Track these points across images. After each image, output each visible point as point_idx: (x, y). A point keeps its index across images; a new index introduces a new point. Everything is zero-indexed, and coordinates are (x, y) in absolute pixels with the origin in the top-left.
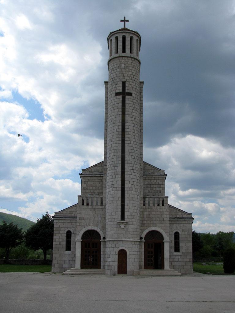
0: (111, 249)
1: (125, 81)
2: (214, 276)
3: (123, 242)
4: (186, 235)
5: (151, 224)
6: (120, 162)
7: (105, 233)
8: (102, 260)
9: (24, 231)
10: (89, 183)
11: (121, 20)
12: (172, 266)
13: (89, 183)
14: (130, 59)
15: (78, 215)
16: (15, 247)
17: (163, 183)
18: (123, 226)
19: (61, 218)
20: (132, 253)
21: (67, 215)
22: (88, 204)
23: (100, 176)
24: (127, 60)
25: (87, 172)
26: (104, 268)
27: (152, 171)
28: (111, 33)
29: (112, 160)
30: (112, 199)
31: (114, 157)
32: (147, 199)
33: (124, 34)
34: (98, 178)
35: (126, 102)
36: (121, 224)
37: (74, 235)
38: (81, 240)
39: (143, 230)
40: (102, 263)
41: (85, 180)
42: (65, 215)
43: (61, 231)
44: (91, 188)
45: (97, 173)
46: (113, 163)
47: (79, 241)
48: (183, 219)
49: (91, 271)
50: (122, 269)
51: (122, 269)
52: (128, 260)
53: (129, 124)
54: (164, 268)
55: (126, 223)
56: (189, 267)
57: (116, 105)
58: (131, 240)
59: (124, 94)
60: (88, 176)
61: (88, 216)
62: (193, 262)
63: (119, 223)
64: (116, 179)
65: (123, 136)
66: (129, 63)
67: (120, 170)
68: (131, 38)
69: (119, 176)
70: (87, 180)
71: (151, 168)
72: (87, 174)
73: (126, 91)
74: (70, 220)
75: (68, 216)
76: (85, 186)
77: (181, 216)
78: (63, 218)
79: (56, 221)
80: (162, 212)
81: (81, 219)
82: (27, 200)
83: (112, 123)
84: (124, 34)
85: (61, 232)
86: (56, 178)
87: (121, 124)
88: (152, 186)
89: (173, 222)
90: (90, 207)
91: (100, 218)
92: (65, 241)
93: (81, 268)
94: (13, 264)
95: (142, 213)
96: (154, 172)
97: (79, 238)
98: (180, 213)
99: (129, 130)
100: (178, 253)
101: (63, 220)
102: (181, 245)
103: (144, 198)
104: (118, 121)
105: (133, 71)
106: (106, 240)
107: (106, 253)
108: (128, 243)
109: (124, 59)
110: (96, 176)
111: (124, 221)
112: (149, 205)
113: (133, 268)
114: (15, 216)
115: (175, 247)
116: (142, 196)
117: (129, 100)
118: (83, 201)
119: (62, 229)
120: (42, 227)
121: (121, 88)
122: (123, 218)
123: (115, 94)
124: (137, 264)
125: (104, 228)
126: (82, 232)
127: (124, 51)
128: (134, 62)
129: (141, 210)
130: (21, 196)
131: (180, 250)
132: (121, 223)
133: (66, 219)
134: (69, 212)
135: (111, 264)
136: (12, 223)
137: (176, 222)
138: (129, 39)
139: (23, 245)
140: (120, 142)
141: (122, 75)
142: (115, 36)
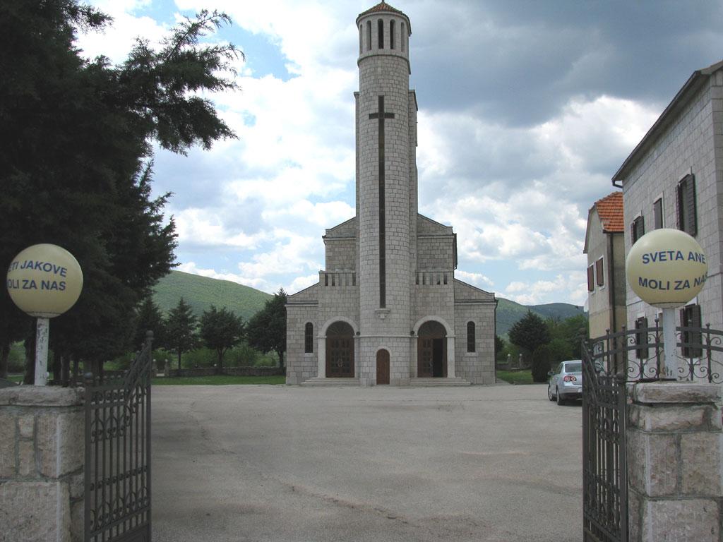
0: (366, 349)
7: (359, 325)
8: (356, 364)
9: (245, 322)
12: (457, 372)
14: (391, 58)
15: (320, 301)
16: (231, 348)
18: (382, 316)
20: (397, 354)
21: (305, 300)
22: (333, 284)
24: (386, 61)
26: (359, 377)
27: (433, 229)
28: (360, 15)
30: (367, 277)
32: (421, 275)
33: (381, 17)
35: (386, 129)
37: (316, 329)
39: (416, 321)
40: (356, 370)
42: (307, 298)
44: (340, 258)
50: (383, 377)
51: (383, 377)
52: (391, 365)
53: (390, 163)
54: (446, 376)
56: (490, 373)
57: (370, 133)
59: (381, 116)
61: (334, 301)
66: (388, 65)
67: (378, 234)
68: (392, 23)
69: (377, 242)
71: (430, 225)
72: (333, 236)
73: (385, 111)
76: (331, 254)
77: (478, 298)
79: (291, 309)
81: (324, 306)
82: (253, 248)
83: (365, 161)
84: (381, 17)
85: (298, 325)
86: (314, 199)
87: (377, 164)
88: (433, 252)
89: (465, 307)
90: (338, 288)
94: (230, 375)
95: (413, 296)
96: (435, 231)
98: (476, 294)
99: (391, 172)
100: (473, 354)
102: (477, 341)
103: (417, 273)
104: (373, 159)
105: (395, 78)
106: (361, 336)
108: (391, 340)
109: (381, 60)
111: (384, 309)
113: (398, 376)
114: (231, 283)
115: (468, 344)
116: (413, 270)
117: (390, 125)
118: (327, 277)
119: (299, 320)
120: (275, 314)
121: (377, 106)
122: (383, 303)
123: (368, 116)
124: (406, 370)
125: (357, 318)
126: (327, 325)
127: (381, 45)
128: (396, 62)
129: (413, 291)
130: (242, 240)
131: (476, 349)
135: (367, 370)
136: (225, 308)
137: (469, 307)
138: (389, 25)
139: (245, 344)
140: (377, 191)
142: (366, 20)
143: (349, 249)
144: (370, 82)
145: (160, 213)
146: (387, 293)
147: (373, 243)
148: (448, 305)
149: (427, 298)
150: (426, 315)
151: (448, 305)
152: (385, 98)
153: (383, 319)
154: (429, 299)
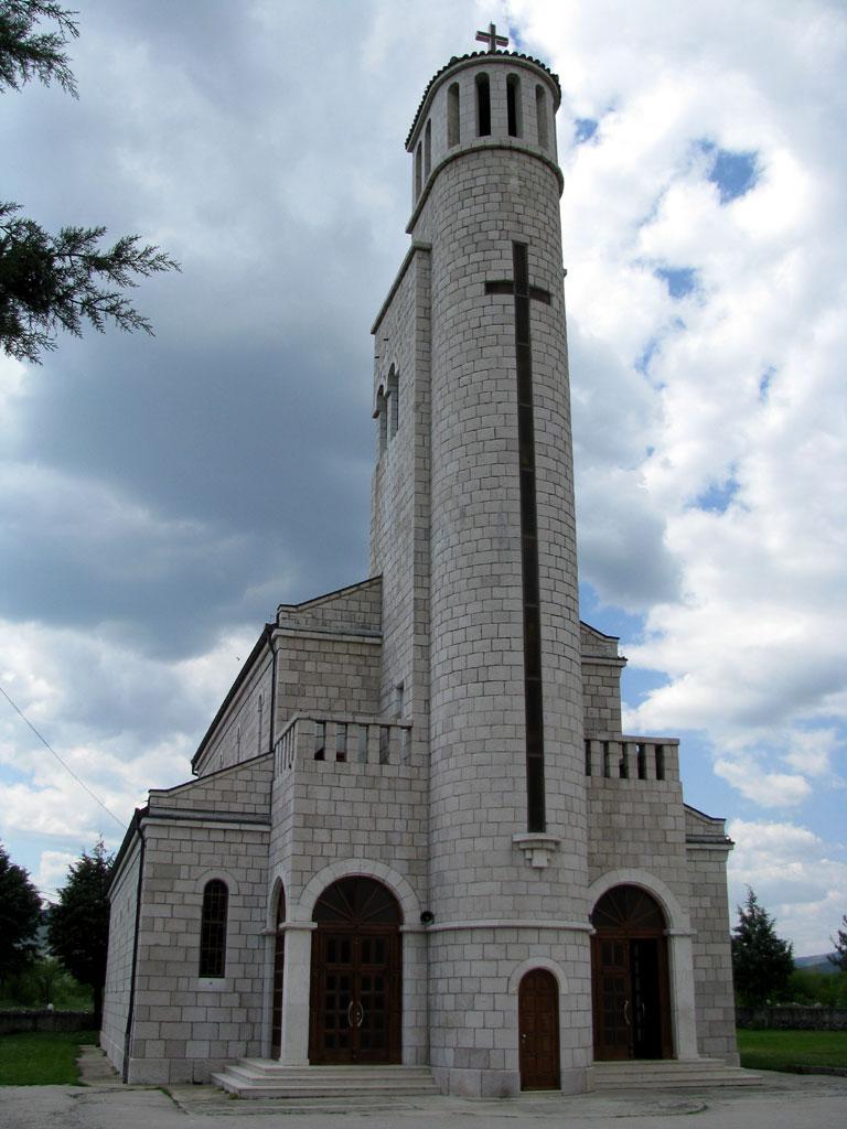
0: (480, 968)
1: (526, 244)
2: (271, 1033)
3: (544, 934)
4: (706, 908)
6: (518, 569)
10: (309, 666)
11: (480, 33)
17: (615, 690)
18: (540, 859)
19: (178, 818)
21: (209, 807)
23: (360, 639)
25: (303, 621)
29: (479, 558)
35: (533, 325)
36: (532, 850)
38: (315, 925)
41: (293, 655)
44: (320, 691)
45: (347, 627)
46: (486, 570)
48: (698, 842)
49: (369, 1075)
55: (552, 846)
58: (495, 923)
60: (308, 635)
61: (343, 810)
62: (740, 1025)
63: (522, 846)
64: (504, 644)
65: (526, 462)
70: (303, 656)
72: (303, 626)
73: (531, 280)
74: (225, 830)
78: (188, 819)
79: (162, 833)
80: (659, 803)
85: (180, 886)
87: (514, 408)
91: (398, 822)
92: (199, 930)
93: (311, 1064)
97: (300, 913)
101: (191, 828)
106: (432, 927)
107: (442, 986)
109: (518, 161)
112: (606, 774)
117: (544, 317)
119: (184, 870)
121: (510, 265)
122: (537, 820)
123: (483, 287)
125: (421, 865)
126: (316, 887)
132: (535, 845)
133: (206, 825)
134: (216, 796)
135: (484, 1040)
138: (494, 122)
141: (514, 217)
142: (475, 71)
143: (346, 669)
146: (549, 786)
147: (504, 630)
149: (615, 817)
150: (613, 868)
152: (530, 249)
153: (540, 869)
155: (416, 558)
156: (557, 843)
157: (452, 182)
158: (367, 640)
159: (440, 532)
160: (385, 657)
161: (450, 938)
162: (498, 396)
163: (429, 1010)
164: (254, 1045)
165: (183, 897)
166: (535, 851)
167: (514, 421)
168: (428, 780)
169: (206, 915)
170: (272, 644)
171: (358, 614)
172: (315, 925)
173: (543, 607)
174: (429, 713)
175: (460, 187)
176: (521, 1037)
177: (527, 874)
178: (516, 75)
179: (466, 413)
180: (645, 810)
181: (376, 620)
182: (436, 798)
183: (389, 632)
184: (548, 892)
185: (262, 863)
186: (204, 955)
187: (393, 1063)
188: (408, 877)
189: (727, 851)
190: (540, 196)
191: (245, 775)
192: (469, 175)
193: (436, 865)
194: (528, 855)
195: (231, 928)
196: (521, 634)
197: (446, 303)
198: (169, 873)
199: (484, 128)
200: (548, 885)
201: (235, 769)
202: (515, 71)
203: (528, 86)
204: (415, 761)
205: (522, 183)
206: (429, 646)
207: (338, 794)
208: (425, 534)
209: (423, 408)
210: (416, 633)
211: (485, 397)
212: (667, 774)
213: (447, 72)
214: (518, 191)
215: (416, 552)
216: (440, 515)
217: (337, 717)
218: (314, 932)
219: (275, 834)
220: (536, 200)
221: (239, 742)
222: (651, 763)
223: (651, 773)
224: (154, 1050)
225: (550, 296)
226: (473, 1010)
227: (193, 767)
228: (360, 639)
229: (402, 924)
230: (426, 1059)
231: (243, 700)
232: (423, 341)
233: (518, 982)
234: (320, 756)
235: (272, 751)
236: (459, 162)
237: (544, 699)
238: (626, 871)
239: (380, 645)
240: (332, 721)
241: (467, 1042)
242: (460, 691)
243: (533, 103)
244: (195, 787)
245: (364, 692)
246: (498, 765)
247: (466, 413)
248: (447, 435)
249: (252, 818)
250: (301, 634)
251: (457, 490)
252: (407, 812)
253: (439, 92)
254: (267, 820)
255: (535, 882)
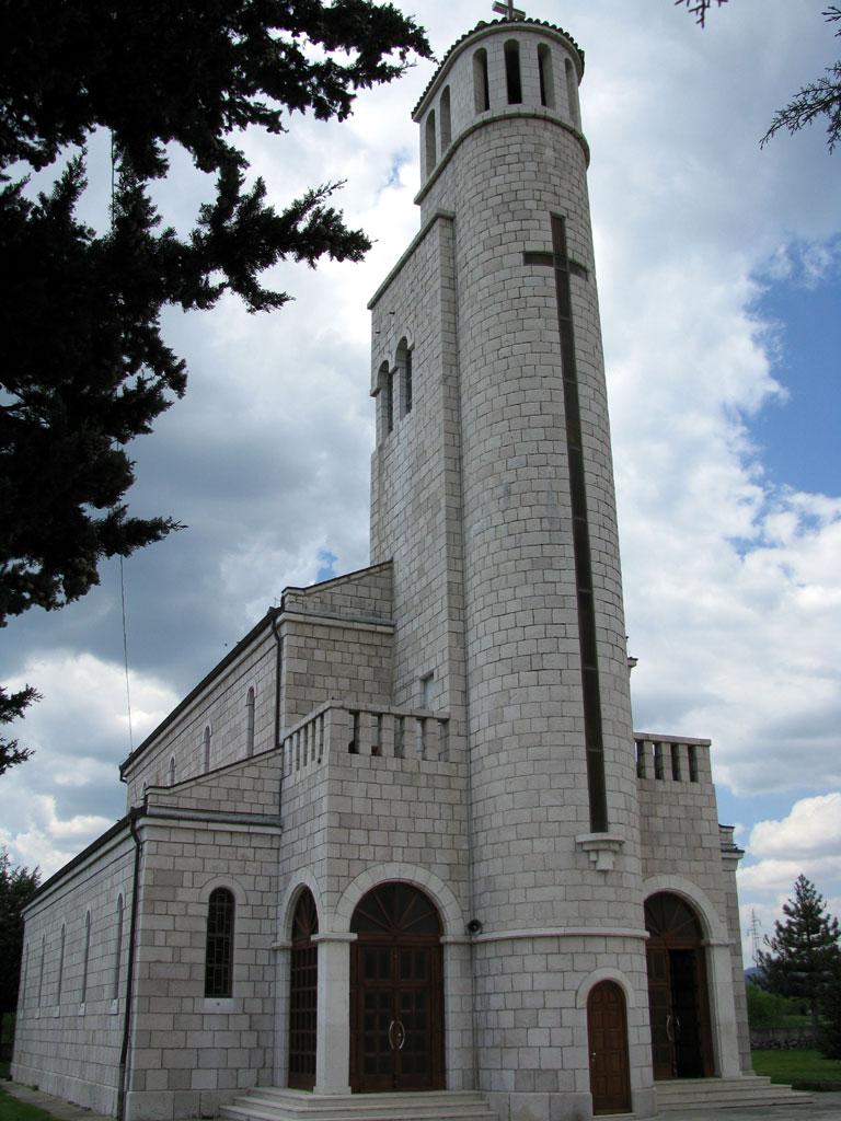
0: (543, 981)
2: (288, 1060)
3: (519, 946)
5: (657, 862)
6: (570, 551)
11: (497, 3)
13: (319, 655)
18: (605, 862)
19: (179, 819)
23: (371, 627)
25: (311, 606)
31: (533, 525)
34: (365, 639)
35: (574, 299)
36: (597, 851)
38: (355, 936)
41: (301, 642)
43: (180, 890)
44: (330, 682)
46: (536, 552)
47: (340, 941)
58: (560, 931)
60: (319, 620)
61: (380, 808)
63: (586, 847)
64: (560, 631)
65: (573, 440)
70: (312, 643)
72: (312, 611)
73: (570, 254)
74: (231, 833)
75: (219, 812)
85: (183, 895)
87: (560, 383)
92: (204, 945)
93: (353, 1092)
97: (334, 924)
106: (481, 937)
110: (357, 626)
121: (549, 236)
122: (599, 820)
125: (465, 867)
126: (355, 894)
133: (212, 826)
134: (222, 795)
135: (550, 1059)
138: (525, 91)
142: (505, 38)
143: (357, 659)
144: (524, 175)
145: (84, 179)
147: (558, 616)
148: (705, 844)
150: (675, 872)
151: (705, 844)
152: (567, 223)
153: (605, 872)
154: (657, 823)
155: (448, 539)
156: (621, 843)
157: (483, 149)
158: (379, 629)
159: (479, 510)
160: (399, 647)
161: (506, 948)
162: (542, 370)
163: (476, 1030)
164: (265, 1074)
165: (186, 907)
166: (600, 853)
167: (560, 396)
168: (469, 777)
169: (211, 928)
170: (276, 629)
171: (367, 601)
172: (355, 936)
173: (597, 593)
174: (467, 705)
175: (492, 154)
176: (591, 1057)
177: (592, 878)
178: (546, 46)
179: (506, 387)
180: (678, 812)
181: (387, 607)
182: (483, 796)
183: (404, 620)
184: (613, 897)
185: (272, 869)
186: (209, 972)
187: (437, 1089)
188: (449, 883)
189: (736, 860)
190: (574, 171)
191: (252, 772)
192: (501, 142)
193: (481, 870)
194: (593, 857)
195: (239, 941)
196: (576, 620)
197: (478, 272)
198: (169, 881)
199: (515, 95)
200: (612, 889)
201: (242, 765)
202: (545, 41)
203: (558, 57)
204: (453, 756)
205: (557, 155)
206: (465, 632)
207: (374, 791)
208: (458, 513)
209: (451, 382)
210: (451, 619)
211: (529, 370)
212: (700, 775)
213: (473, 36)
214: (553, 163)
215: (448, 532)
216: (474, 490)
217: (371, 707)
218: (352, 944)
219: (287, 838)
220: (570, 173)
221: (208, 742)
222: (684, 764)
223: (685, 774)
224: (157, 1081)
225: (585, 271)
226: (537, 1027)
227: (122, 772)
228: (371, 627)
229: (442, 935)
230: (475, 1082)
231: (216, 695)
232: (449, 312)
233: (586, 995)
234: (353, 748)
235: (279, 746)
236: (490, 128)
237: (601, 689)
238: (665, 877)
239: (392, 634)
240: (366, 712)
241: (530, 1062)
242: (510, 680)
243: (564, 76)
244: (199, 784)
245: (376, 685)
246: (557, 759)
247: (506, 387)
248: (483, 409)
249: (261, 819)
250: (311, 620)
251: (499, 466)
252: (446, 812)
253: (464, 55)
254: (276, 822)
255: (599, 886)
